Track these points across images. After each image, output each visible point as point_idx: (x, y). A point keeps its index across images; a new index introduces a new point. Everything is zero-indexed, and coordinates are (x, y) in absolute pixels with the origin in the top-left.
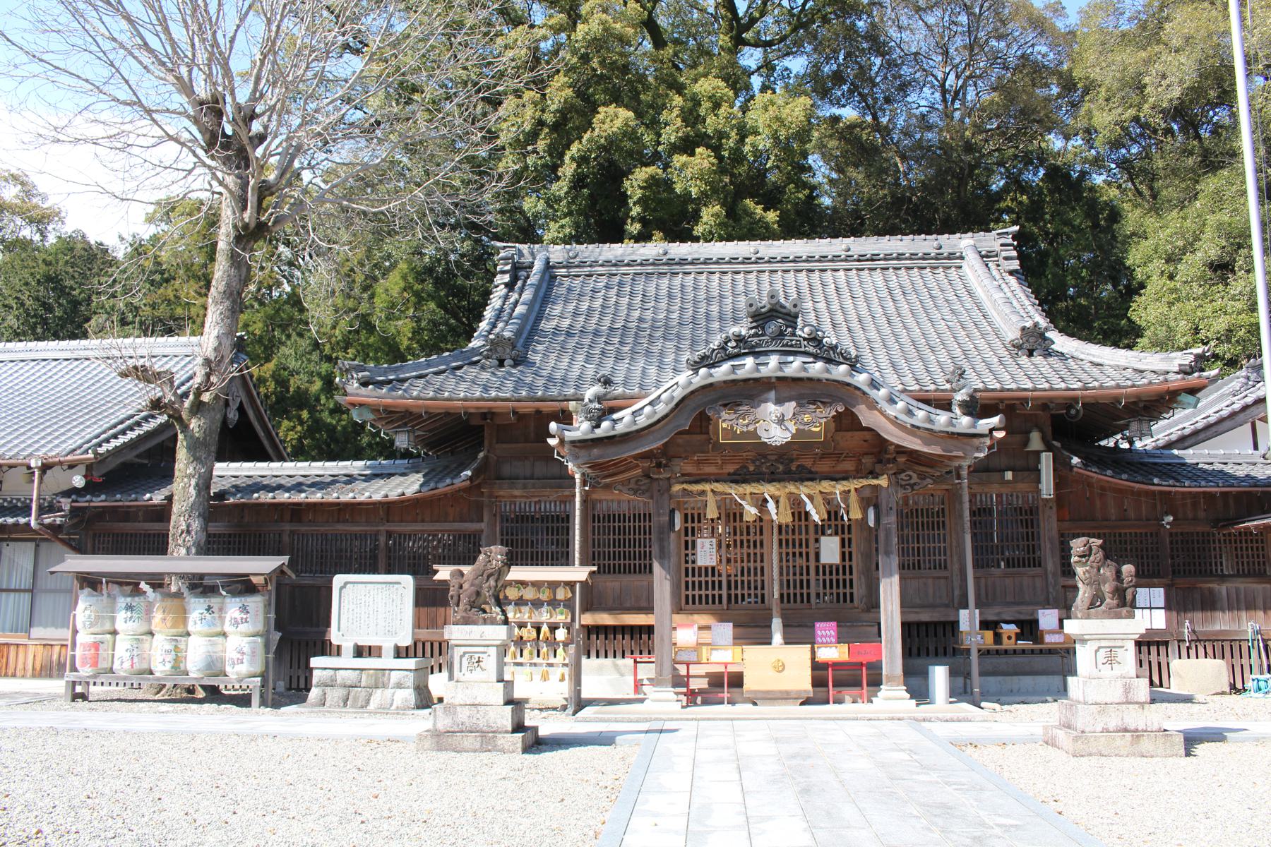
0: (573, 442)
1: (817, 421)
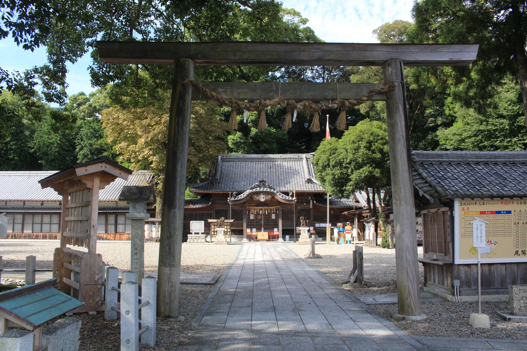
1: (269, 197)
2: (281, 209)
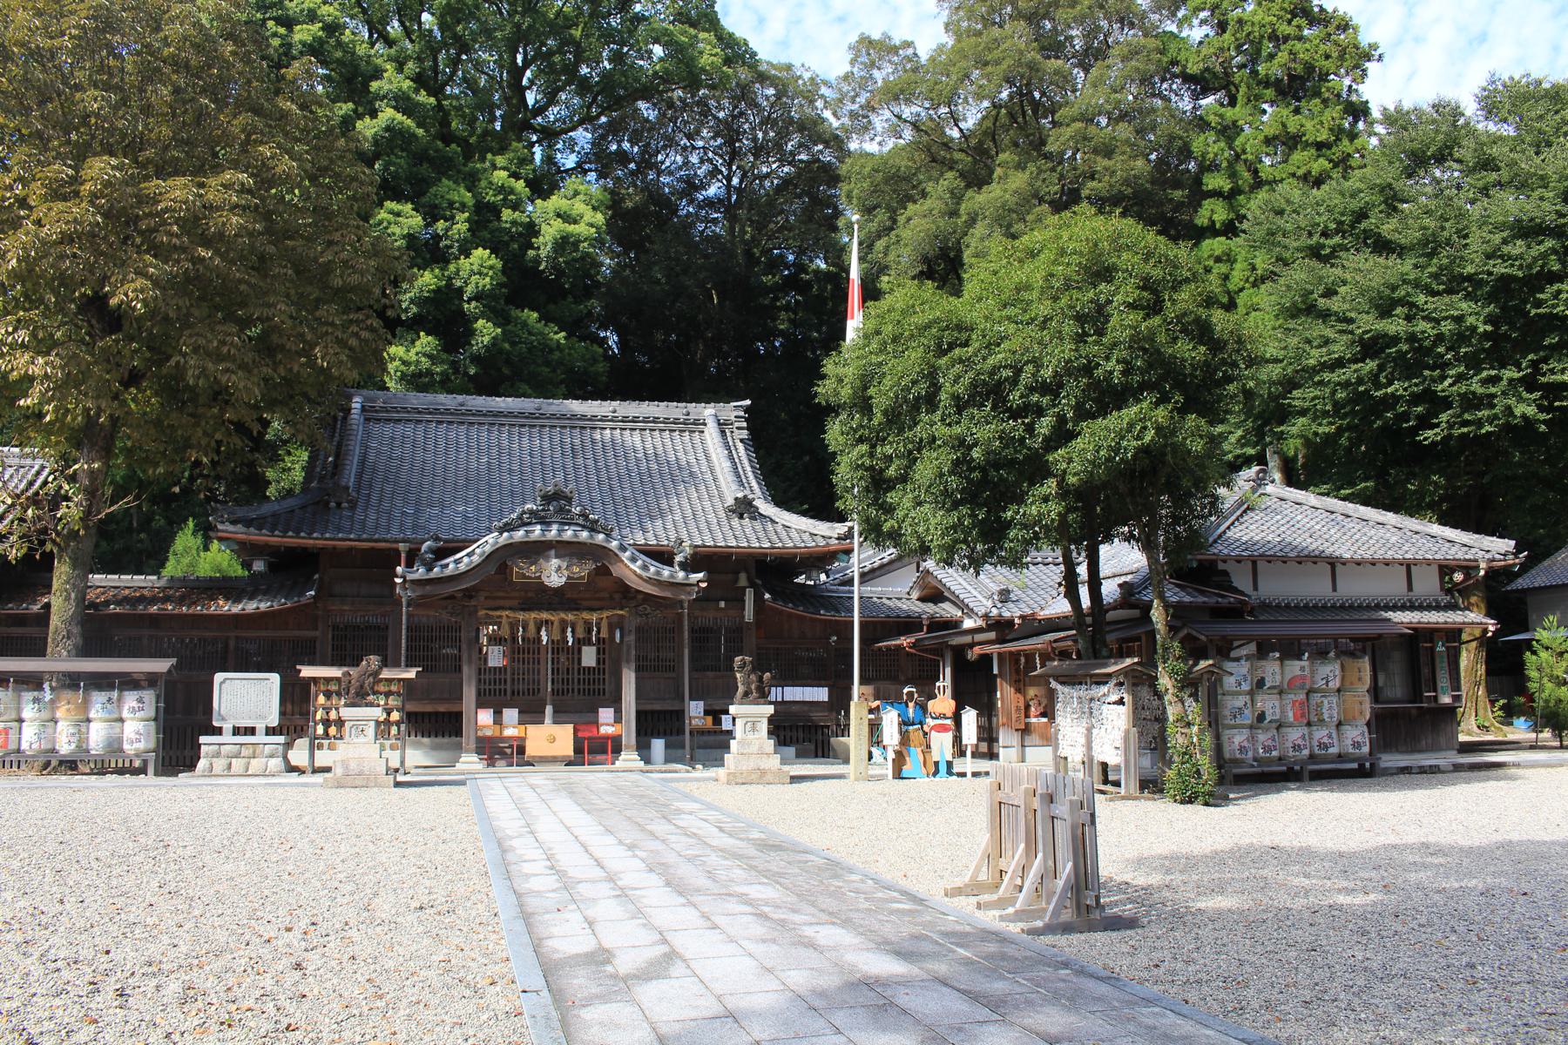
0: (413, 581)
1: (582, 570)
2: (633, 622)
